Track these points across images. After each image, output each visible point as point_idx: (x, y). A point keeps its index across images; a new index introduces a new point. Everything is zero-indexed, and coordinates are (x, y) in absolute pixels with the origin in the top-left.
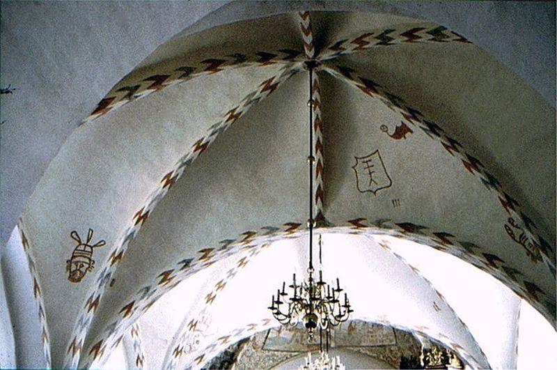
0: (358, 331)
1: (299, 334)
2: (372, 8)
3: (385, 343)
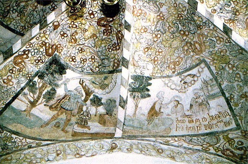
0: (164, 116)
1: (63, 116)
2: (172, 159)
3: (215, 129)
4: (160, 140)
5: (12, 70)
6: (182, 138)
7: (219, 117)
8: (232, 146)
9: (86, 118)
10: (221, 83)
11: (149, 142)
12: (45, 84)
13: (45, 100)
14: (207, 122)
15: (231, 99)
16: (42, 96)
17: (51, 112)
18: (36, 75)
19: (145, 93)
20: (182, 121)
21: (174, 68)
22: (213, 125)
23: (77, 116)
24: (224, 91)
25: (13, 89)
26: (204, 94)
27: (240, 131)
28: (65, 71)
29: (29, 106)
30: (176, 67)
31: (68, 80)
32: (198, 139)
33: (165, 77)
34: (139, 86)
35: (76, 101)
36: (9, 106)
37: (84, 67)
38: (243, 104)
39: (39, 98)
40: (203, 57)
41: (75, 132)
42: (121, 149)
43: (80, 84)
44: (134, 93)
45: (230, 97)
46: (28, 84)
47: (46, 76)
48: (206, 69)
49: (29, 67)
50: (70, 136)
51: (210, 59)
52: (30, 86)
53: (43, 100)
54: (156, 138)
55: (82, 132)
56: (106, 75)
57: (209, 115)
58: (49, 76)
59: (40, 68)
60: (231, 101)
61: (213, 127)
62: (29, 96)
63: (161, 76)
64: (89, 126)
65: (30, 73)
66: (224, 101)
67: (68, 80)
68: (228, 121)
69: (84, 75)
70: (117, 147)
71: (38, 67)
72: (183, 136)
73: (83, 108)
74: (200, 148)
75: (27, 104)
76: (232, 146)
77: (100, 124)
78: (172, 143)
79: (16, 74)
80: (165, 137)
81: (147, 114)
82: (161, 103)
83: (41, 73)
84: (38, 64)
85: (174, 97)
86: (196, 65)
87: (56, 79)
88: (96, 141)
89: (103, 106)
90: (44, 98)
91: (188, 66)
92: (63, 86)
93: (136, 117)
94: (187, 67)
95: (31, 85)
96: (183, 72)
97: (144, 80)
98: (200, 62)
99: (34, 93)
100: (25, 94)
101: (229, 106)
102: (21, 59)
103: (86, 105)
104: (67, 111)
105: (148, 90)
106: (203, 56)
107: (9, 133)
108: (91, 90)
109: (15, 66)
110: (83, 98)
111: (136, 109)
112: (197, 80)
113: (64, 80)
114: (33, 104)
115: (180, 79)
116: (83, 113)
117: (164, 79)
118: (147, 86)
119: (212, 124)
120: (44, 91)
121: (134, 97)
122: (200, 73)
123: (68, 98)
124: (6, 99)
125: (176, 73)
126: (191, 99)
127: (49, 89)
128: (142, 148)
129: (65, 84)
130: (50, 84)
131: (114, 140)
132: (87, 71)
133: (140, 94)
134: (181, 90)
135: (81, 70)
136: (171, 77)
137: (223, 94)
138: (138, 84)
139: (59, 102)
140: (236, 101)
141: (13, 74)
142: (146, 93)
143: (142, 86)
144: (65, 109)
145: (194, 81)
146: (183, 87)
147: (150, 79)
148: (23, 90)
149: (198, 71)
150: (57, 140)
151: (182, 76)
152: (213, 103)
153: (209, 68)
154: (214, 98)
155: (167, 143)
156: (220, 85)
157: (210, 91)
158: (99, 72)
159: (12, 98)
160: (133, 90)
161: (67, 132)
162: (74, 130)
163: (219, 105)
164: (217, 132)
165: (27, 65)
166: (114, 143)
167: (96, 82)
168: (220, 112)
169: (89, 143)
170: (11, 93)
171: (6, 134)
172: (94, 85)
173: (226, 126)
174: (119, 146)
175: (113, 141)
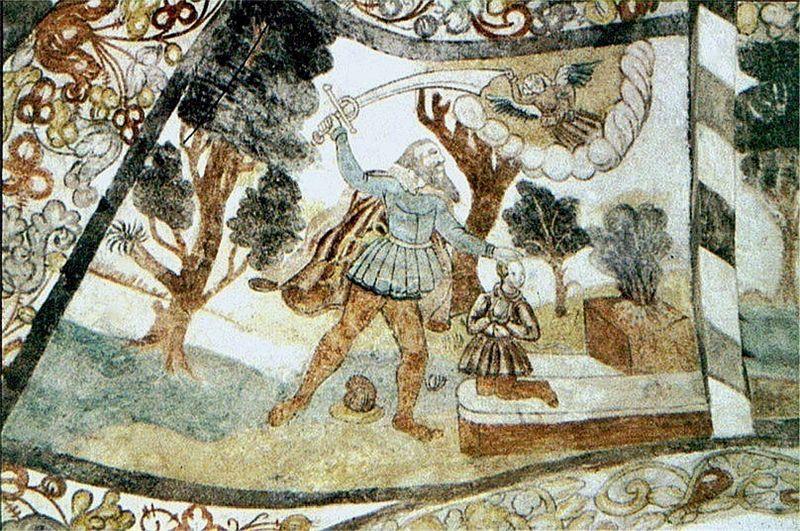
1: (377, 338)
5: (34, 100)
9: (512, 333)
12: (225, 154)
13: (248, 250)
16: (227, 232)
17: (301, 320)
18: (168, 102)
23: (457, 326)
25: (54, 215)
28: (325, 52)
29: (166, 304)
31: (349, 108)
35: (425, 231)
36: (56, 327)
37: (430, 12)
39: (209, 244)
41: (475, 428)
42: (745, 496)
43: (425, 121)
46: (130, 172)
47: (227, 103)
49: (124, 62)
50: (459, 458)
52: (146, 181)
53: (234, 251)
55: (515, 420)
56: (580, 55)
58: (237, 96)
59: (182, 59)
62: (151, 245)
64: (547, 384)
65: (133, 102)
67: (347, 107)
69: (439, 65)
71: (174, 55)
73: (475, 276)
75: (153, 293)
79: (60, 118)
83: (192, 84)
84: (170, 32)
87: (278, 112)
90: (242, 243)
92: (328, 148)
95: (150, 173)
99: (175, 217)
100: (129, 237)
102: (74, 22)
103: (490, 250)
104: (390, 304)
107: (99, 493)
108: (499, 159)
109: (47, 74)
110: (463, 211)
111: (792, 248)
113: (325, 108)
114: (187, 287)
116: (489, 305)
120: (226, 195)
121: (769, 182)
123: (375, 221)
124: (30, 286)
127: (251, 178)
129: (340, 137)
130: (253, 150)
131: (713, 457)
132: (455, 32)
135: (412, 34)
139: (331, 254)
141: (43, 122)
144: (372, 290)
148: (112, 213)
150: (392, 493)
158: (529, 34)
159: (64, 270)
161: (430, 433)
162: (469, 417)
165: (106, 47)
166: (713, 471)
167: (520, 101)
169: (579, 484)
170: (52, 238)
171: (82, 501)
172: (512, 121)
174: (738, 481)
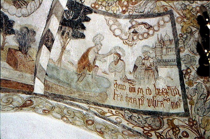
0: (99, 73)
3: (159, 109)
4: (94, 109)
6: (121, 112)
7: (167, 93)
8: (177, 135)
10: (182, 50)
11: (81, 110)
14: (152, 95)
15: (186, 74)
19: (78, 30)
20: (121, 86)
21: (127, 7)
22: (159, 102)
24: (181, 61)
26: (156, 56)
27: (187, 119)
30: (130, 5)
32: (139, 118)
33: (110, 15)
34: (72, 18)
38: (199, 85)
40: (172, 7)
44: (64, 27)
45: (186, 70)
48: (170, 24)
51: (180, 14)
54: (89, 105)
57: (155, 86)
60: (185, 77)
61: (158, 105)
63: (105, 11)
66: (177, 73)
68: (176, 102)
70: (33, 105)
72: (122, 109)
74: (140, 130)
76: (177, 135)
77: (10, 65)
78: (109, 116)
80: (100, 105)
81: (77, 63)
82: (97, 52)
85: (115, 48)
86: (158, 13)
88: (7, 93)
89: (14, 35)
91: (146, 11)
93: (62, 65)
94: (145, 13)
96: (137, 17)
97: (82, 11)
98: (165, 13)
101: (182, 82)
105: (84, 28)
106: (173, 6)
112: (153, 35)
115: (130, 25)
117: (108, 18)
118: (84, 21)
119: (156, 101)
122: (159, 27)
125: (127, 14)
126: (137, 58)
128: (67, 114)
133: (71, 30)
134: (127, 41)
136: (119, 18)
137: (179, 65)
138: (73, 14)
140: (191, 78)
142: (81, 31)
143: (76, 20)
145: (148, 34)
146: (131, 37)
147: (90, 11)
149: (158, 23)
151: (134, 21)
152: (163, 72)
153: (174, 25)
154: (166, 66)
155: (102, 115)
156: (178, 52)
157: (164, 54)
160: (64, 23)
163: (170, 77)
164: (161, 113)
168: (169, 87)
173: (173, 108)
175: (30, 97)
